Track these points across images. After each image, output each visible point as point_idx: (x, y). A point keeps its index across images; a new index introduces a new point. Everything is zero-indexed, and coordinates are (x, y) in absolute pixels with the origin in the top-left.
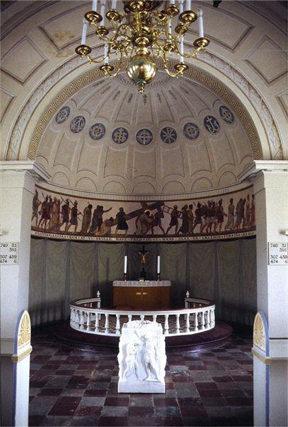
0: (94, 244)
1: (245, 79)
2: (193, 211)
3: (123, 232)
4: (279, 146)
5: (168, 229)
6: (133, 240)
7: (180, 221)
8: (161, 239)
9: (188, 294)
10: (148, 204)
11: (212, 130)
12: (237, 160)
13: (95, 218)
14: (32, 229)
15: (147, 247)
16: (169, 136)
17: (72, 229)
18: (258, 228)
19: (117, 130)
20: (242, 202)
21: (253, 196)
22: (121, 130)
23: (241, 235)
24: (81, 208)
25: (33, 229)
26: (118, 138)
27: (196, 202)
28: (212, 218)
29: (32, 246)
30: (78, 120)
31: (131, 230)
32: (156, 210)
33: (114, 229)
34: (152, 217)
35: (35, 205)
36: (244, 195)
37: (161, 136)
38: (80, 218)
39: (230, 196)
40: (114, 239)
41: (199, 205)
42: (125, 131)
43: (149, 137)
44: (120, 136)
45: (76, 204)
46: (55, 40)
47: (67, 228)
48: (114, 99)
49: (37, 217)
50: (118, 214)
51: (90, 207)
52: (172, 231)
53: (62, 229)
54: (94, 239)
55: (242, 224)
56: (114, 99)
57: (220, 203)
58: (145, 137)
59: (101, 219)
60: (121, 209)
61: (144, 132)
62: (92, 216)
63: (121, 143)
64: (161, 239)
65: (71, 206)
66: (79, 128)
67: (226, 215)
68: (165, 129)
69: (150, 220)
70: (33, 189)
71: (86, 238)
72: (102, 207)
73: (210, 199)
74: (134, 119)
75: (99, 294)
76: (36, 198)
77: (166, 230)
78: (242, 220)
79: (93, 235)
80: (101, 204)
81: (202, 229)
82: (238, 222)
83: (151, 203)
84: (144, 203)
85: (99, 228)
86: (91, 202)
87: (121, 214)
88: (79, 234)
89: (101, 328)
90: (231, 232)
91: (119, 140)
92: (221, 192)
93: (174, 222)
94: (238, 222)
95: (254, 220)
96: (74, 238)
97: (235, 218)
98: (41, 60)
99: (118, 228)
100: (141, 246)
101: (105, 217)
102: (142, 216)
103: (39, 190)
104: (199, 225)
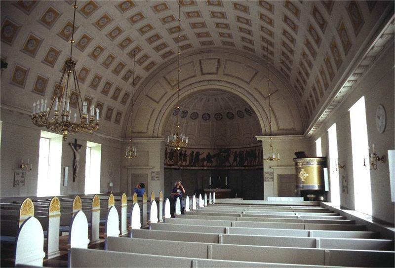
1: (254, 97)
7: (238, 159)
13: (195, 158)
14: (165, 165)
17: (184, 164)
18: (163, 169)
31: (214, 164)
33: (205, 163)
35: (166, 154)
38: (188, 158)
40: (205, 168)
41: (247, 151)
44: (206, 117)
45: (185, 151)
46: (171, 82)
51: (193, 152)
52: (235, 164)
53: (179, 164)
54: (195, 168)
57: (255, 150)
58: (218, 116)
60: (209, 153)
65: (183, 152)
68: (228, 113)
71: (192, 168)
72: (199, 153)
79: (195, 166)
80: (198, 150)
81: (248, 163)
86: (194, 150)
87: (209, 155)
88: (188, 166)
93: (235, 160)
98: (164, 92)
99: (208, 163)
103: (167, 147)
104: (247, 162)
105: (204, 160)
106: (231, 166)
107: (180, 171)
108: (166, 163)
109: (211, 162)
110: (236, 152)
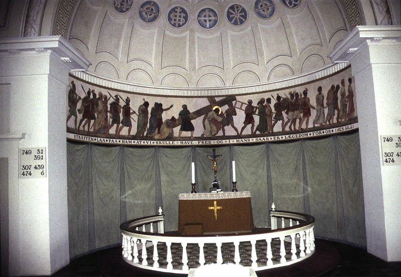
0: (153, 149)
2: (272, 105)
3: (187, 134)
4: (385, 9)
5: (243, 129)
6: (201, 143)
7: (257, 119)
8: (235, 141)
9: (273, 206)
10: (217, 99)
12: (326, 39)
15: (219, 151)
16: (237, 15)
17: (124, 131)
20: (334, 90)
21: (350, 80)
22: (179, 10)
23: (335, 130)
24: (135, 106)
25: (69, 130)
26: (175, 20)
27: (275, 94)
28: (296, 112)
29: (70, 153)
32: (226, 107)
33: (177, 130)
34: (222, 114)
36: (336, 81)
37: (228, 17)
39: (318, 84)
40: (176, 143)
41: (279, 98)
42: (183, 11)
43: (213, 18)
45: (128, 101)
47: (118, 130)
49: (76, 117)
50: (181, 112)
51: (146, 104)
52: (248, 131)
53: (112, 131)
55: (335, 117)
57: (305, 93)
59: (161, 119)
60: (185, 107)
61: (207, 13)
62: (149, 116)
63: (179, 26)
64: (235, 141)
65: (122, 103)
66: (125, 6)
67: (314, 108)
69: (220, 119)
70: (67, 81)
71: (142, 143)
72: (161, 105)
73: (292, 90)
75: (160, 211)
76: (72, 93)
77: (239, 131)
78: (336, 112)
79: (152, 139)
81: (284, 126)
82: (331, 116)
83: (223, 98)
84: (211, 99)
85: (159, 130)
86: (147, 99)
87: (185, 112)
88: (134, 138)
89: (150, 261)
90: (322, 128)
92: (305, 80)
93: (249, 120)
94: (331, 116)
95: (352, 109)
96: (127, 142)
97: (326, 111)
99: (182, 129)
100: (211, 150)
101: (165, 116)
102: (210, 114)
104: (280, 122)
105: (172, 122)
106: (239, 136)
107: (115, 150)
108: (72, 124)
109: (191, 128)
110: (250, 102)
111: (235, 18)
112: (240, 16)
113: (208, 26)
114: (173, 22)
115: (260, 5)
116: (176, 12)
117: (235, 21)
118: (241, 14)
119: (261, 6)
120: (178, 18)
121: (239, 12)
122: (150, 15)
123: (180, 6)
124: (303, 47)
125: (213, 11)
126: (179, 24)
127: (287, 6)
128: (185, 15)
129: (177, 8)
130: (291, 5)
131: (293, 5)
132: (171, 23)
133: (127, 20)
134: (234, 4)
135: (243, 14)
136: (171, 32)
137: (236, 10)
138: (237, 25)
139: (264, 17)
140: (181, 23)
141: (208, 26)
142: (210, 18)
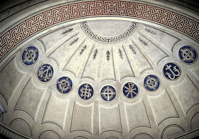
11: (172, 76)
16: (131, 91)
19: (83, 86)
22: (87, 86)
26: (84, 94)
30: (46, 68)
37: (124, 92)
42: (90, 87)
43: (112, 93)
48: (81, 53)
56: (81, 53)
61: (108, 89)
63: (87, 98)
66: (46, 77)
68: (127, 85)
74: (99, 76)
83: (4, 9)
91: (85, 95)
111: (129, 93)
112: (133, 91)
113: (108, 99)
114: (82, 95)
115: (150, 87)
116: (85, 88)
117: (129, 95)
118: (133, 90)
119: (149, 82)
120: (86, 92)
121: (132, 87)
122: (65, 88)
123: (88, 83)
124: (187, 108)
125: (112, 88)
126: (86, 97)
127: (170, 79)
128: (91, 90)
129: (85, 84)
130: (172, 78)
131: (174, 78)
132: (80, 96)
133: (47, 88)
134: (128, 82)
135: (135, 89)
136: (80, 102)
137: (130, 86)
138: (131, 98)
139: (151, 90)
140: (88, 96)
141: (108, 99)
142: (110, 93)
